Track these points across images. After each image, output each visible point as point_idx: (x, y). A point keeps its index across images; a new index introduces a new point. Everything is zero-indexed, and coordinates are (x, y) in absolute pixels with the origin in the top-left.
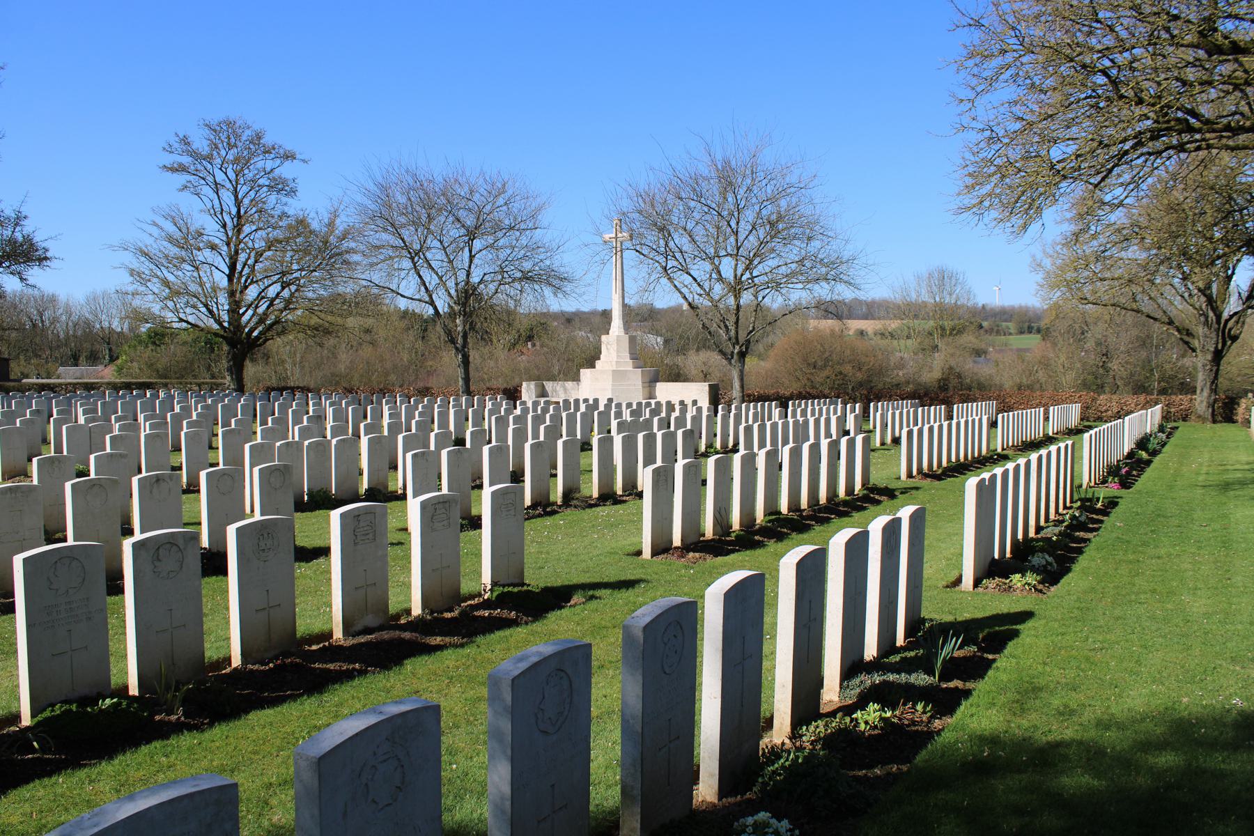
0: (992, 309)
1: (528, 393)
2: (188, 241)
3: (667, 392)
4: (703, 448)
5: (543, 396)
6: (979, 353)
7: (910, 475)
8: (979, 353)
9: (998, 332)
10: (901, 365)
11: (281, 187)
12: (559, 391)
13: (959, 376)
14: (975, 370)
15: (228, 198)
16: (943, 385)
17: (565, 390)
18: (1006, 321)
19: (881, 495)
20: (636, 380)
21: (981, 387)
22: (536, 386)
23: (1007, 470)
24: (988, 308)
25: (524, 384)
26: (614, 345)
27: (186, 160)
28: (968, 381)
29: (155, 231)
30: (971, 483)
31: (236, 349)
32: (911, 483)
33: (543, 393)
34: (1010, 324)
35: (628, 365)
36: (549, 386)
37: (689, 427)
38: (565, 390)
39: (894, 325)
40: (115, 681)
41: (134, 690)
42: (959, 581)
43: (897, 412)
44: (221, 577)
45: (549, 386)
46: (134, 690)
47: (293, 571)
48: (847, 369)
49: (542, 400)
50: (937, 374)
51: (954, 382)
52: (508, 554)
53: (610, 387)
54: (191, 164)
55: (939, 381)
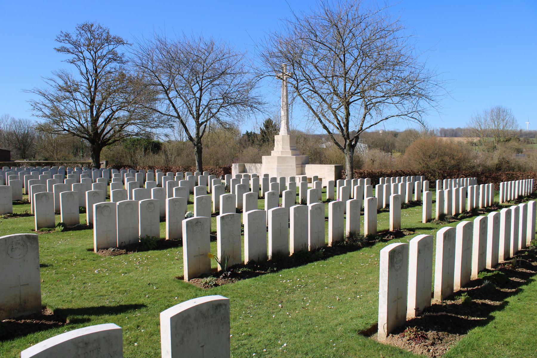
0: (525, 132)
1: (235, 170)
2: (70, 89)
3: (312, 170)
4: (214, 211)
5: (244, 172)
6: (519, 151)
7: (503, 202)
8: (519, 151)
9: (528, 143)
10: (476, 157)
11: (115, 58)
12: (252, 169)
13: (508, 162)
14: (517, 160)
15: (90, 66)
16: (498, 168)
17: (256, 169)
18: (532, 137)
19: (90, 314)
20: (292, 163)
21: (520, 169)
22: (239, 166)
23: (510, 210)
24: (523, 132)
25: (233, 165)
26: (281, 142)
27: (69, 46)
28: (513, 165)
29: (53, 84)
30: (385, 251)
31: (96, 146)
32: (429, 225)
33: (244, 171)
34: (534, 139)
35: (289, 153)
36: (248, 166)
37: (288, 189)
38: (256, 169)
39: (476, 140)
40: (326, 241)
41: (330, 245)
42: (374, 329)
43: (392, 185)
44: (419, 207)
45: (248, 166)
46: (330, 245)
47: (400, 212)
48: (447, 159)
49: (243, 174)
50: (496, 161)
51: (504, 166)
52: (372, 223)
53: (276, 167)
54: (70, 46)
55: (497, 165)
